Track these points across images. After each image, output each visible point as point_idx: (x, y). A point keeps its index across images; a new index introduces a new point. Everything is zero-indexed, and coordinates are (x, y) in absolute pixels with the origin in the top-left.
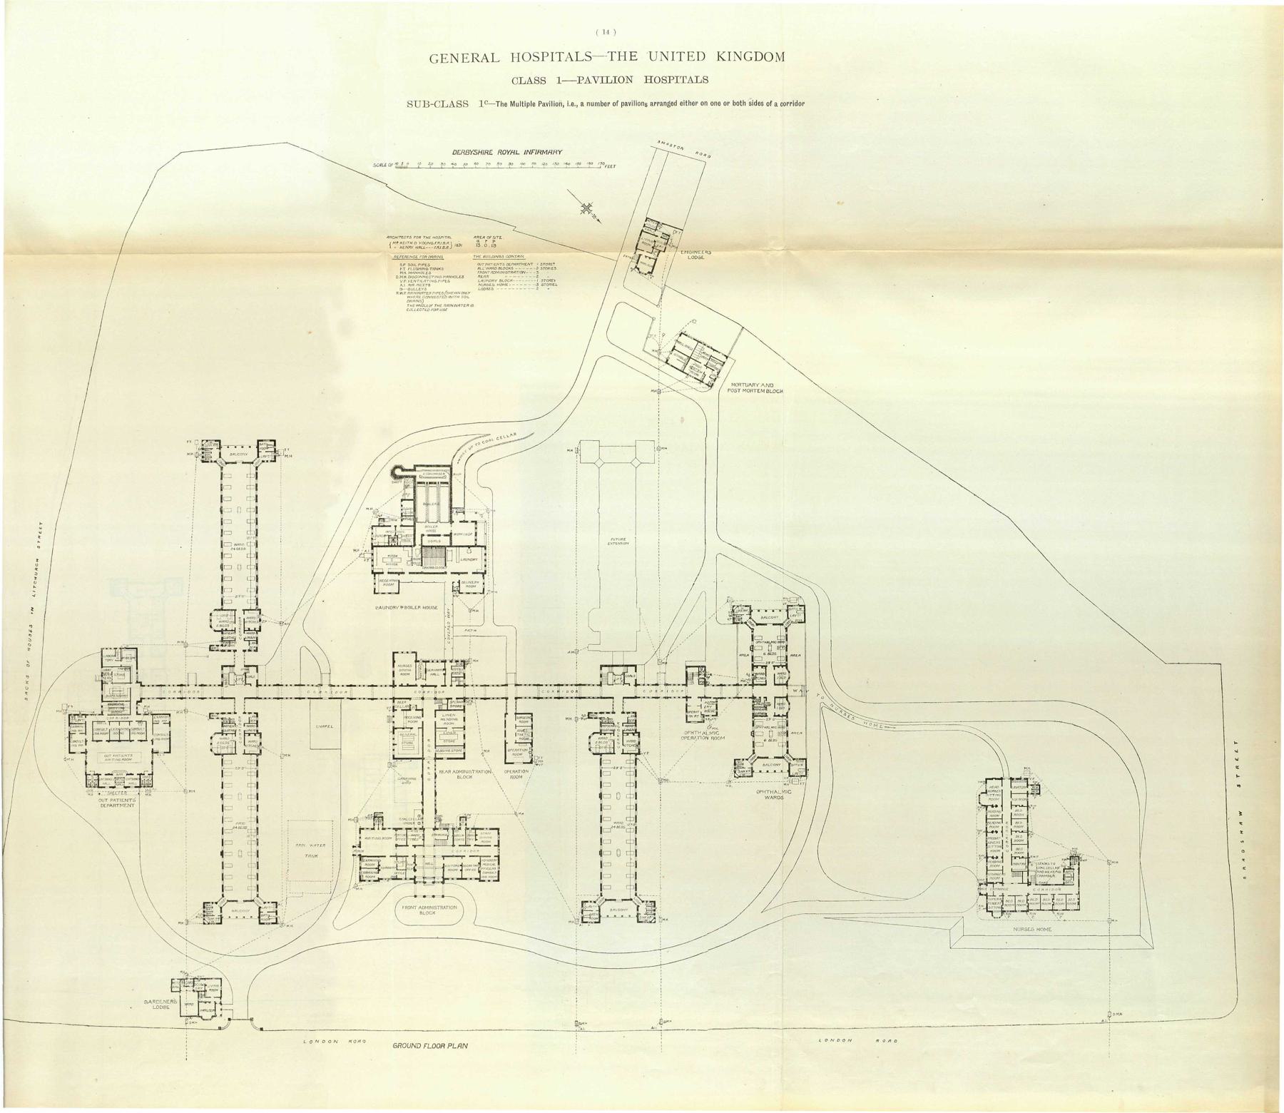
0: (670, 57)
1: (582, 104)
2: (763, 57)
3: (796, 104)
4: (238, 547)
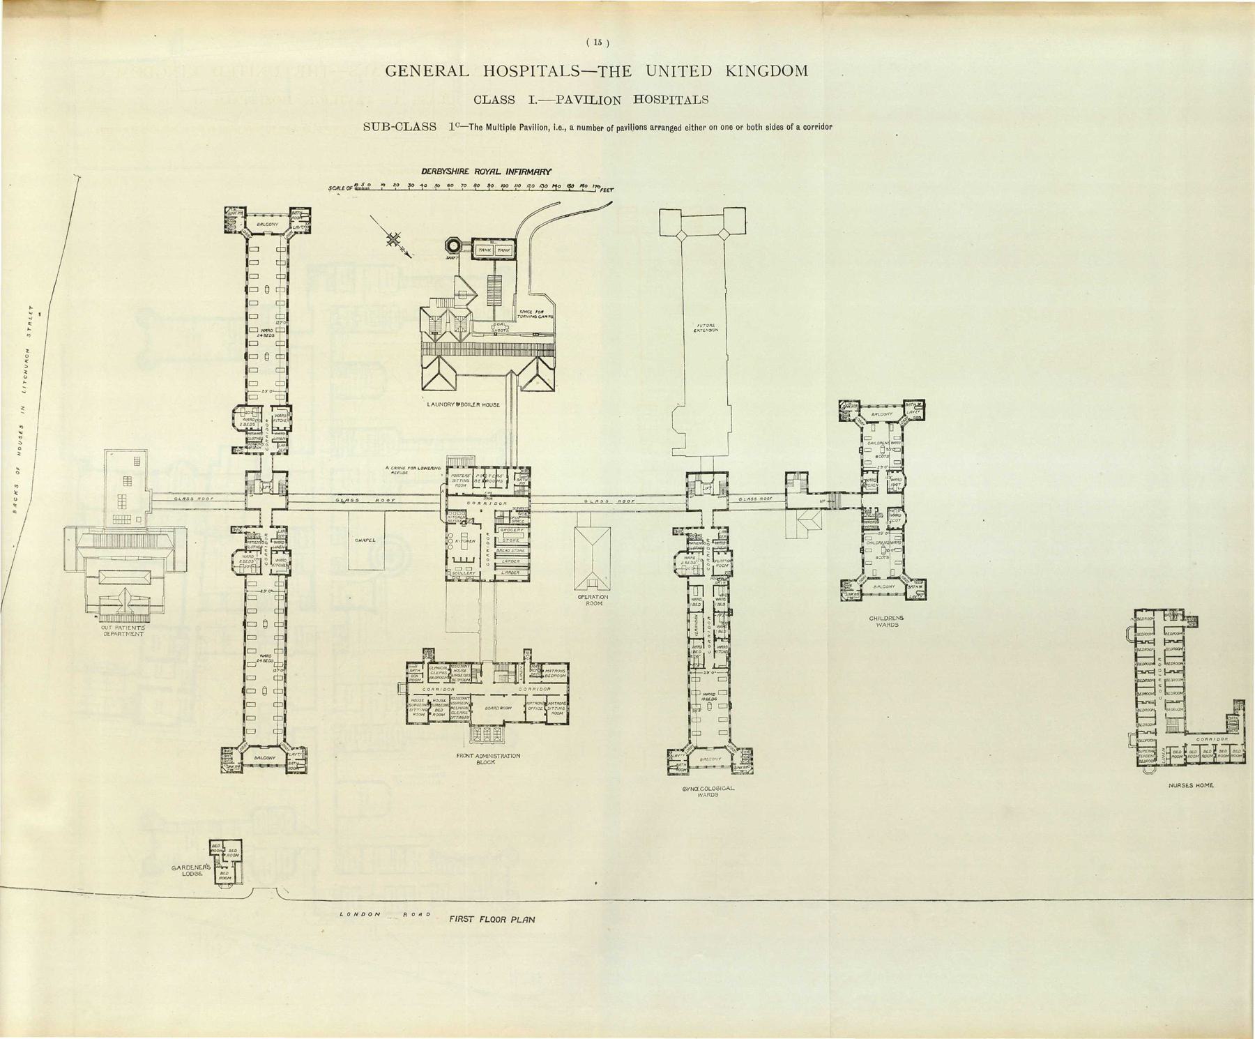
0: (670, 73)
1: (349, 914)
2: (781, 71)
3: (823, 127)
4: (266, 333)
